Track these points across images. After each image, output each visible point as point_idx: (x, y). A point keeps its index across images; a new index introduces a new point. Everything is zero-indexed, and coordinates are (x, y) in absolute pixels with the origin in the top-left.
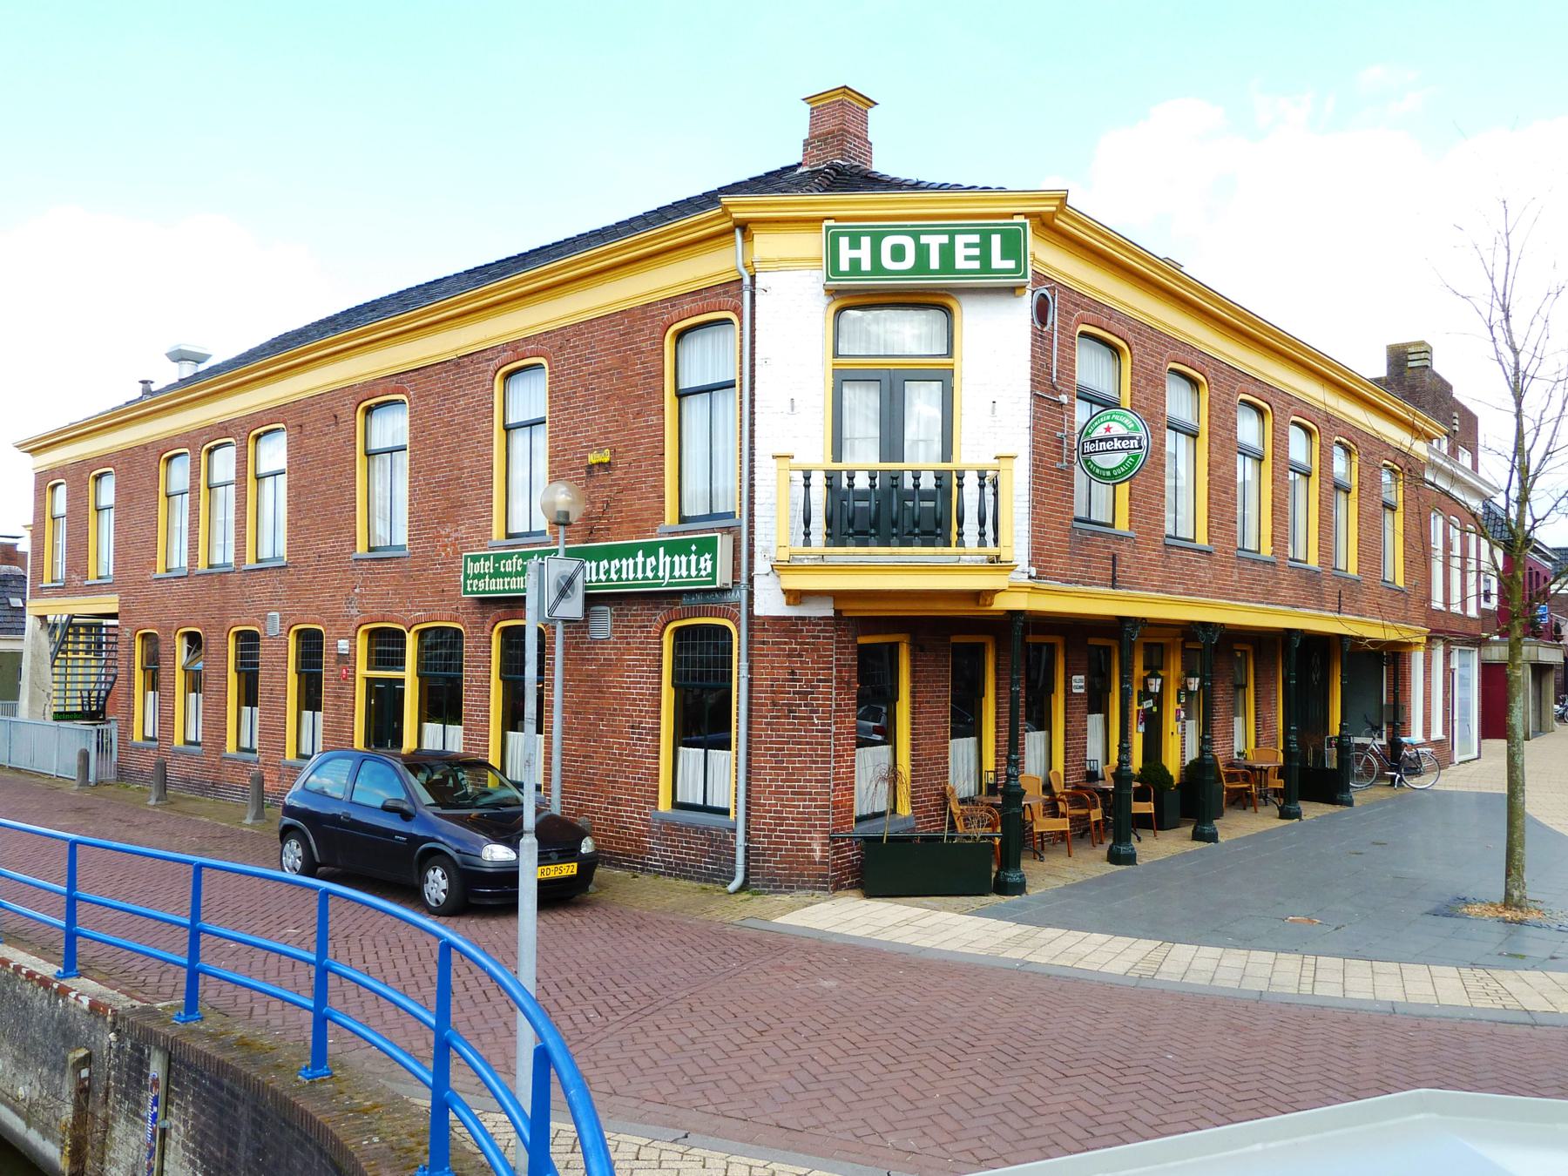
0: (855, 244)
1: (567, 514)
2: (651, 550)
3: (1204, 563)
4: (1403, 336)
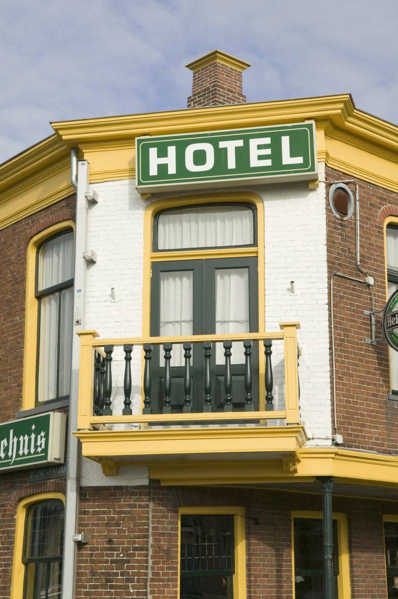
0: (162, 153)
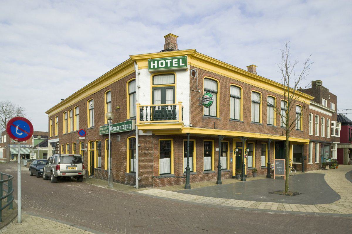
0: (154, 63)
1: (111, 118)
2: (123, 124)
3: (242, 124)
4: (315, 79)
